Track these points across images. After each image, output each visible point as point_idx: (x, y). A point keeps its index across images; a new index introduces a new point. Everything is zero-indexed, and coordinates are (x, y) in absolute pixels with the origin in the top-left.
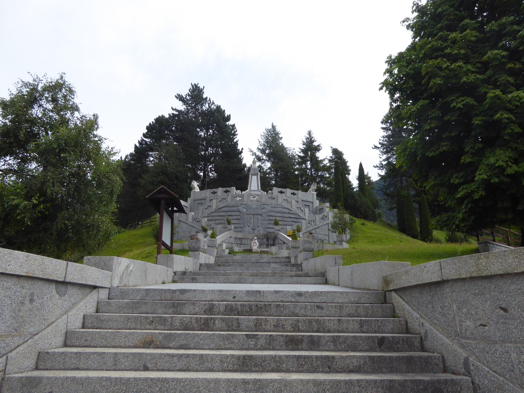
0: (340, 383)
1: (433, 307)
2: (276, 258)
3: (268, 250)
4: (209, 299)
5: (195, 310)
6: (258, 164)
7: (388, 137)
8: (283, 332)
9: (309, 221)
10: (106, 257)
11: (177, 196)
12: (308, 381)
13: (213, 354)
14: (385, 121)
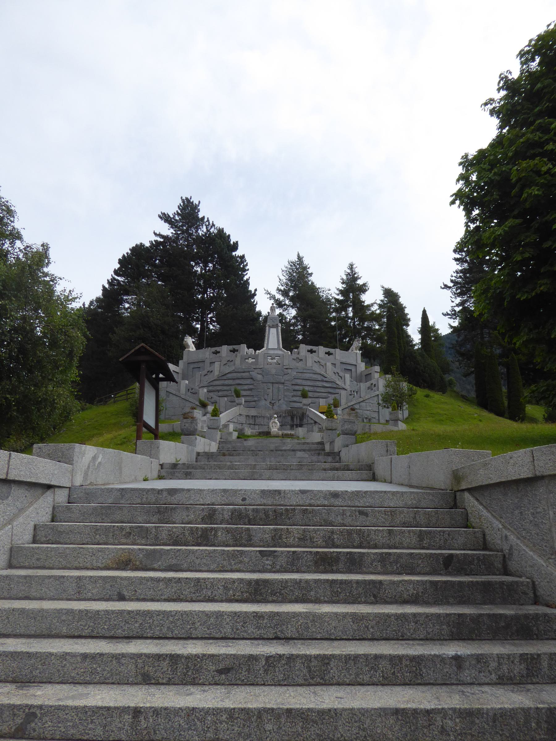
0: (390, 617)
1: (521, 513)
2: (304, 443)
3: (293, 432)
4: (209, 502)
5: (189, 517)
6: (278, 311)
7: (463, 271)
8: (312, 548)
9: (351, 391)
10: (64, 445)
11: (163, 358)
12: (345, 615)
13: (214, 578)
14: (459, 249)
